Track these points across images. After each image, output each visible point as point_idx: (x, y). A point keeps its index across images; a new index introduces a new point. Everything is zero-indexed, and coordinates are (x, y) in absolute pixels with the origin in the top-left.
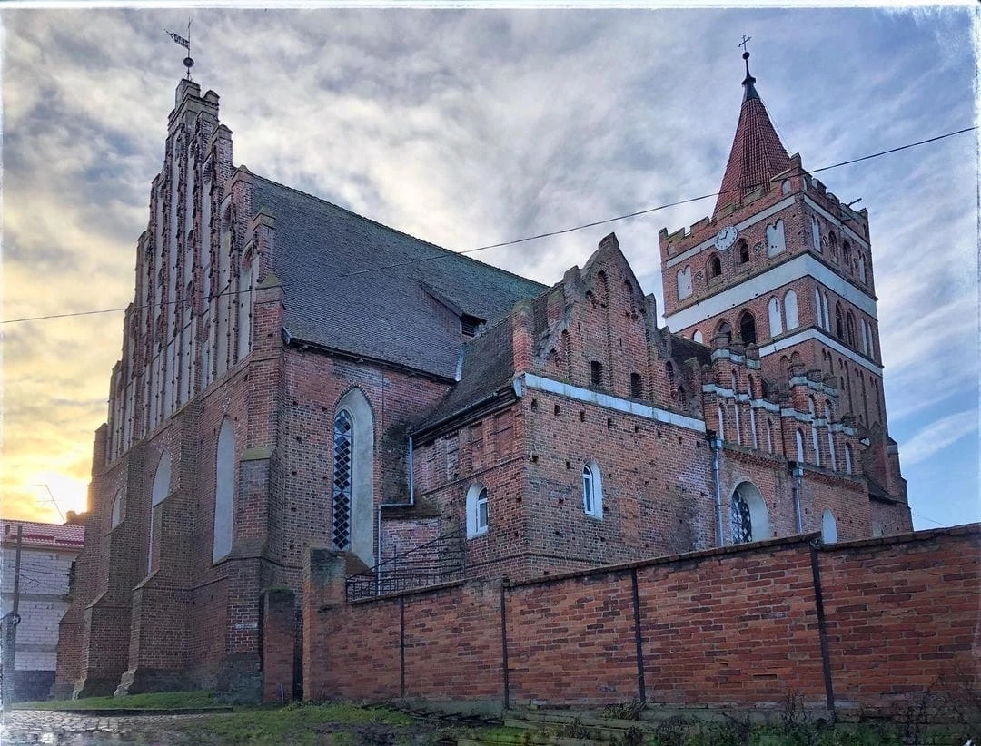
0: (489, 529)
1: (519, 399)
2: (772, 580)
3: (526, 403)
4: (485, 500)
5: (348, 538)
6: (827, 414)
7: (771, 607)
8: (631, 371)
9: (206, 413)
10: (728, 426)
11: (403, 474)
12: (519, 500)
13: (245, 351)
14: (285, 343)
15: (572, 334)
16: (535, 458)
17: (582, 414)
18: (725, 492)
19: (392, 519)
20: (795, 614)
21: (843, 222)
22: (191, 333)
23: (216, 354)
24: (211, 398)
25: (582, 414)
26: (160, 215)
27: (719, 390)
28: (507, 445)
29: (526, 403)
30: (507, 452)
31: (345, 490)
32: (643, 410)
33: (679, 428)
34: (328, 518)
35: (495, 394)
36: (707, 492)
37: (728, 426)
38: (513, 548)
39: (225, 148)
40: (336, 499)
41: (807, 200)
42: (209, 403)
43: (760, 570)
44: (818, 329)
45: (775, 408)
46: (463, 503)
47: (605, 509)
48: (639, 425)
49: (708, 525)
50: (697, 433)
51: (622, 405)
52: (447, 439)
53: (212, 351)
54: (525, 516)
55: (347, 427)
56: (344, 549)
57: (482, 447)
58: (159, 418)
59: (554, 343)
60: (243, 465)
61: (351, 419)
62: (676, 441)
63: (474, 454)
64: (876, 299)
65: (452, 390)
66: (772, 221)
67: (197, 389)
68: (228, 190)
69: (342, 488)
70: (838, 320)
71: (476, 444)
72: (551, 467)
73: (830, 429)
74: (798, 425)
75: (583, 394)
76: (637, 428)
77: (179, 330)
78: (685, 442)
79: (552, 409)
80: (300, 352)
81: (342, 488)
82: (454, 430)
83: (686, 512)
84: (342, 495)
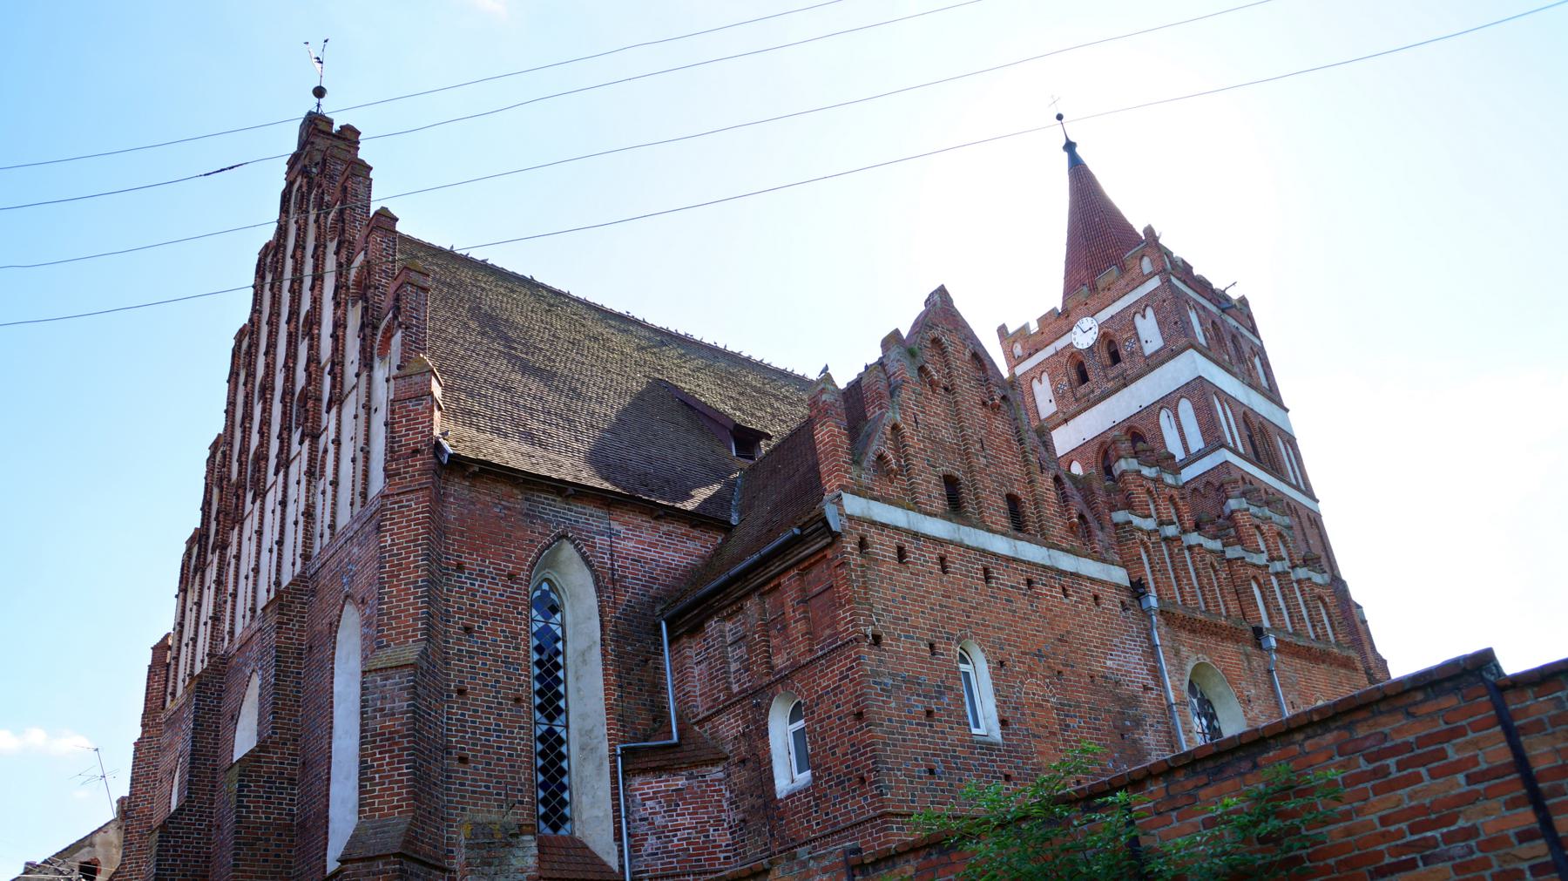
0: (813, 775)
1: (836, 536)
2: (1423, 770)
3: (850, 545)
4: (801, 724)
5: (567, 811)
6: (1284, 553)
7: (1437, 834)
8: (1005, 491)
9: (320, 596)
10: (1159, 575)
11: (658, 688)
12: (859, 716)
13: (378, 483)
14: (440, 463)
15: (907, 431)
16: (877, 639)
17: (942, 559)
18: (1174, 687)
19: (644, 771)
20: (1491, 844)
21: (1223, 311)
22: (297, 469)
23: (335, 496)
24: (325, 570)
25: (942, 559)
26: (267, 295)
27: (1137, 521)
28: (827, 620)
29: (850, 545)
30: (828, 632)
31: (557, 722)
32: (1031, 552)
33: (1092, 580)
34: (528, 776)
35: (797, 531)
36: (1151, 684)
37: (1159, 575)
38: (857, 806)
39: (361, 190)
40: (542, 739)
41: (1174, 280)
42: (324, 579)
43: (1394, 751)
44: (1230, 449)
45: (1216, 545)
46: (764, 733)
47: (1004, 723)
48: (1033, 576)
49: (1162, 737)
50: (1118, 586)
51: (1000, 545)
52: (724, 619)
53: (329, 489)
54: (872, 744)
55: (554, 609)
56: (562, 832)
57: (784, 628)
58: (248, 614)
59: (880, 444)
60: (369, 678)
61: (559, 597)
62: (1091, 600)
63: (774, 642)
64: (1287, 410)
65: (725, 541)
66: (1140, 307)
67: (306, 557)
68: (359, 244)
69: (551, 718)
70: (1250, 437)
71: (775, 625)
72: (904, 653)
73: (1293, 576)
74: (1250, 571)
75: (937, 527)
76: (1030, 582)
77: (284, 463)
78: (1106, 604)
79: (892, 554)
80: (465, 478)
81: (551, 718)
82: (734, 603)
83: (1125, 723)
84: (551, 732)
